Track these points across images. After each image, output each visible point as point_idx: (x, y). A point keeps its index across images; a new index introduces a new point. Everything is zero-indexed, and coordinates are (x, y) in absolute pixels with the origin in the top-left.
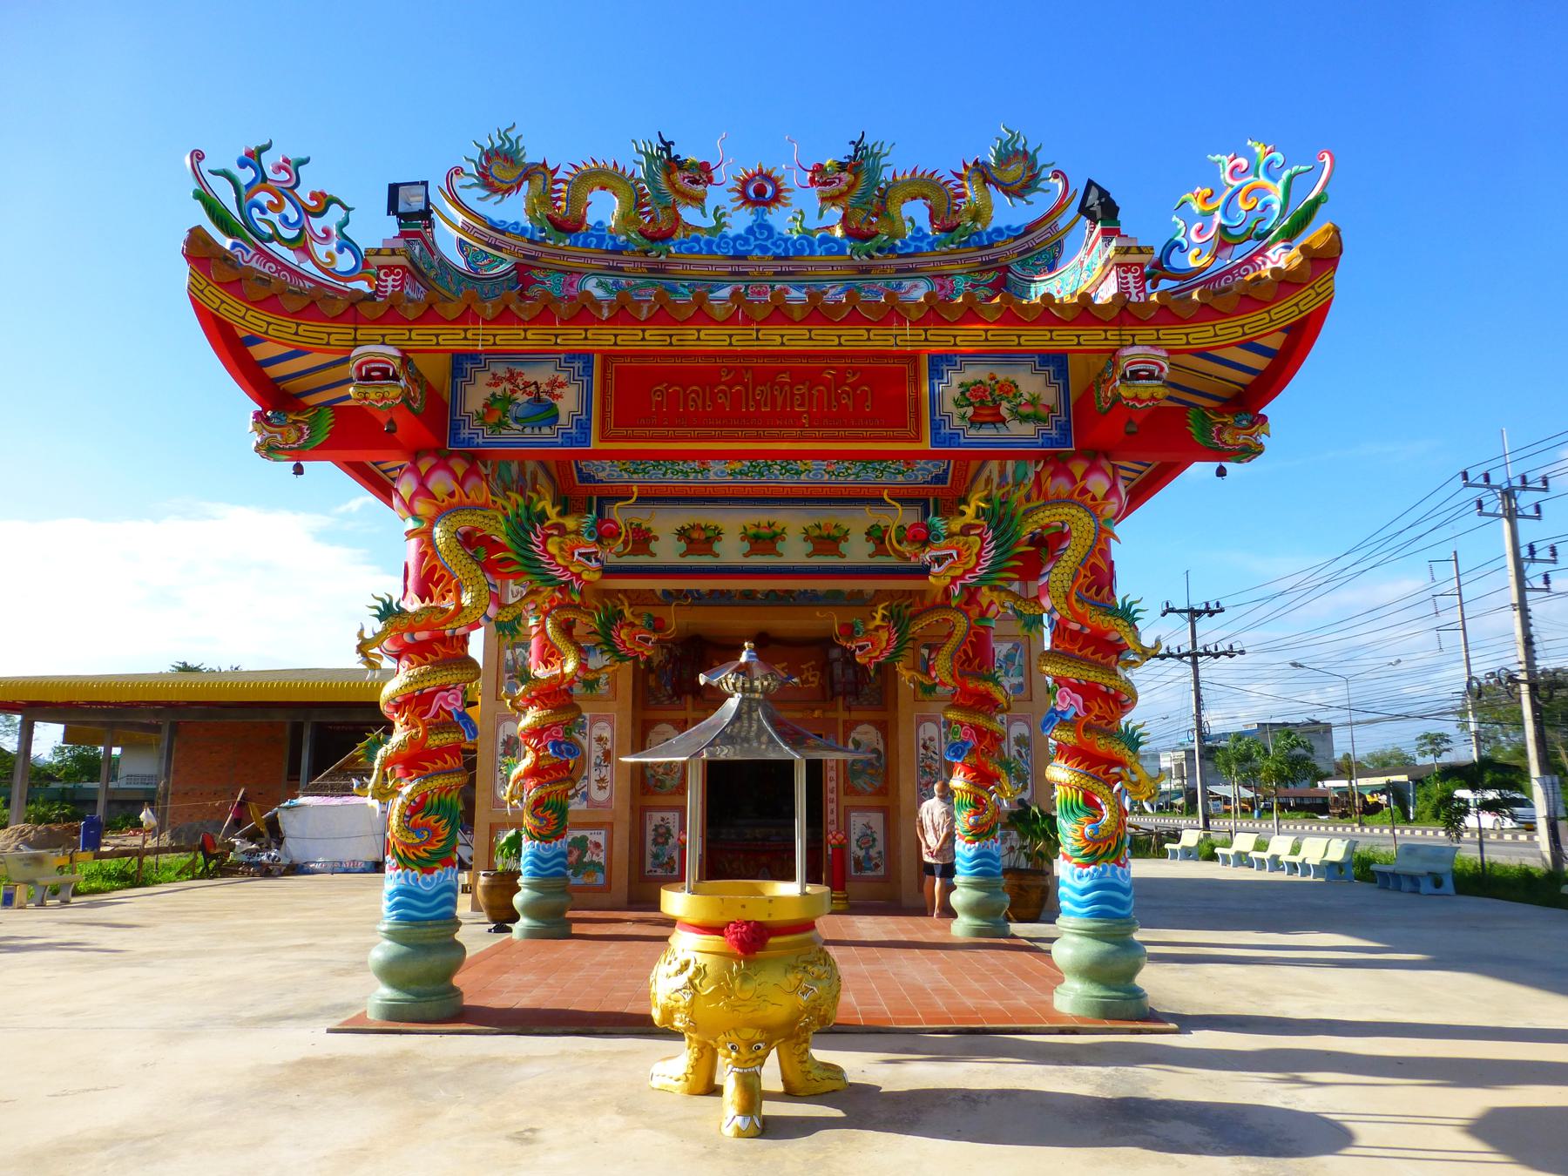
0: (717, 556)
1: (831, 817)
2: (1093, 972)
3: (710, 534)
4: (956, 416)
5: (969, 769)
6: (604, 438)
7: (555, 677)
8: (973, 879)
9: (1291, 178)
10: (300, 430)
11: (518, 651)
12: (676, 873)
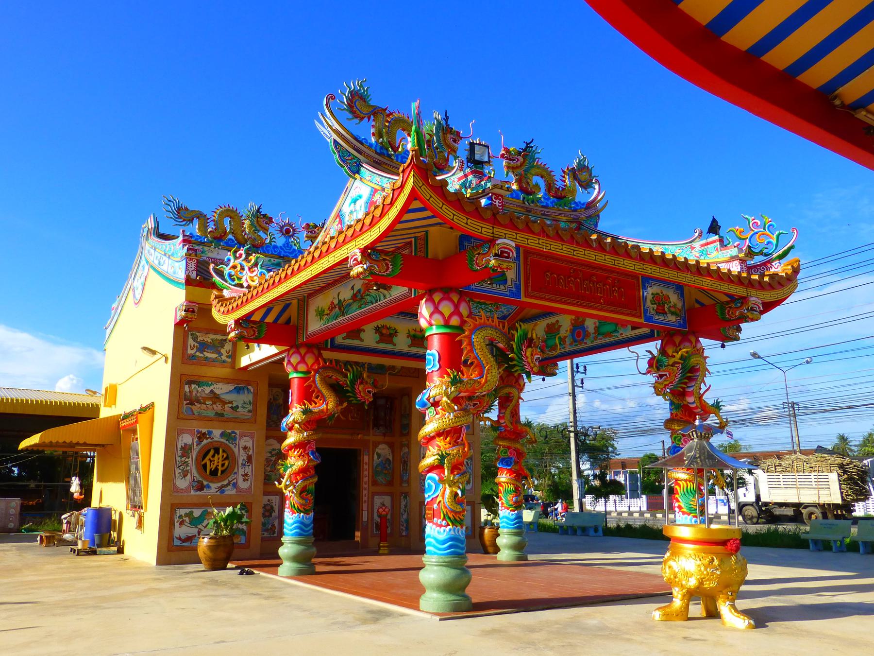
0: (395, 345)
1: (365, 499)
2: (448, 588)
3: (392, 332)
4: (652, 307)
5: (510, 472)
6: (527, 296)
7: (322, 411)
8: (515, 531)
9: (780, 234)
10: (387, 265)
11: (193, 386)
12: (276, 535)
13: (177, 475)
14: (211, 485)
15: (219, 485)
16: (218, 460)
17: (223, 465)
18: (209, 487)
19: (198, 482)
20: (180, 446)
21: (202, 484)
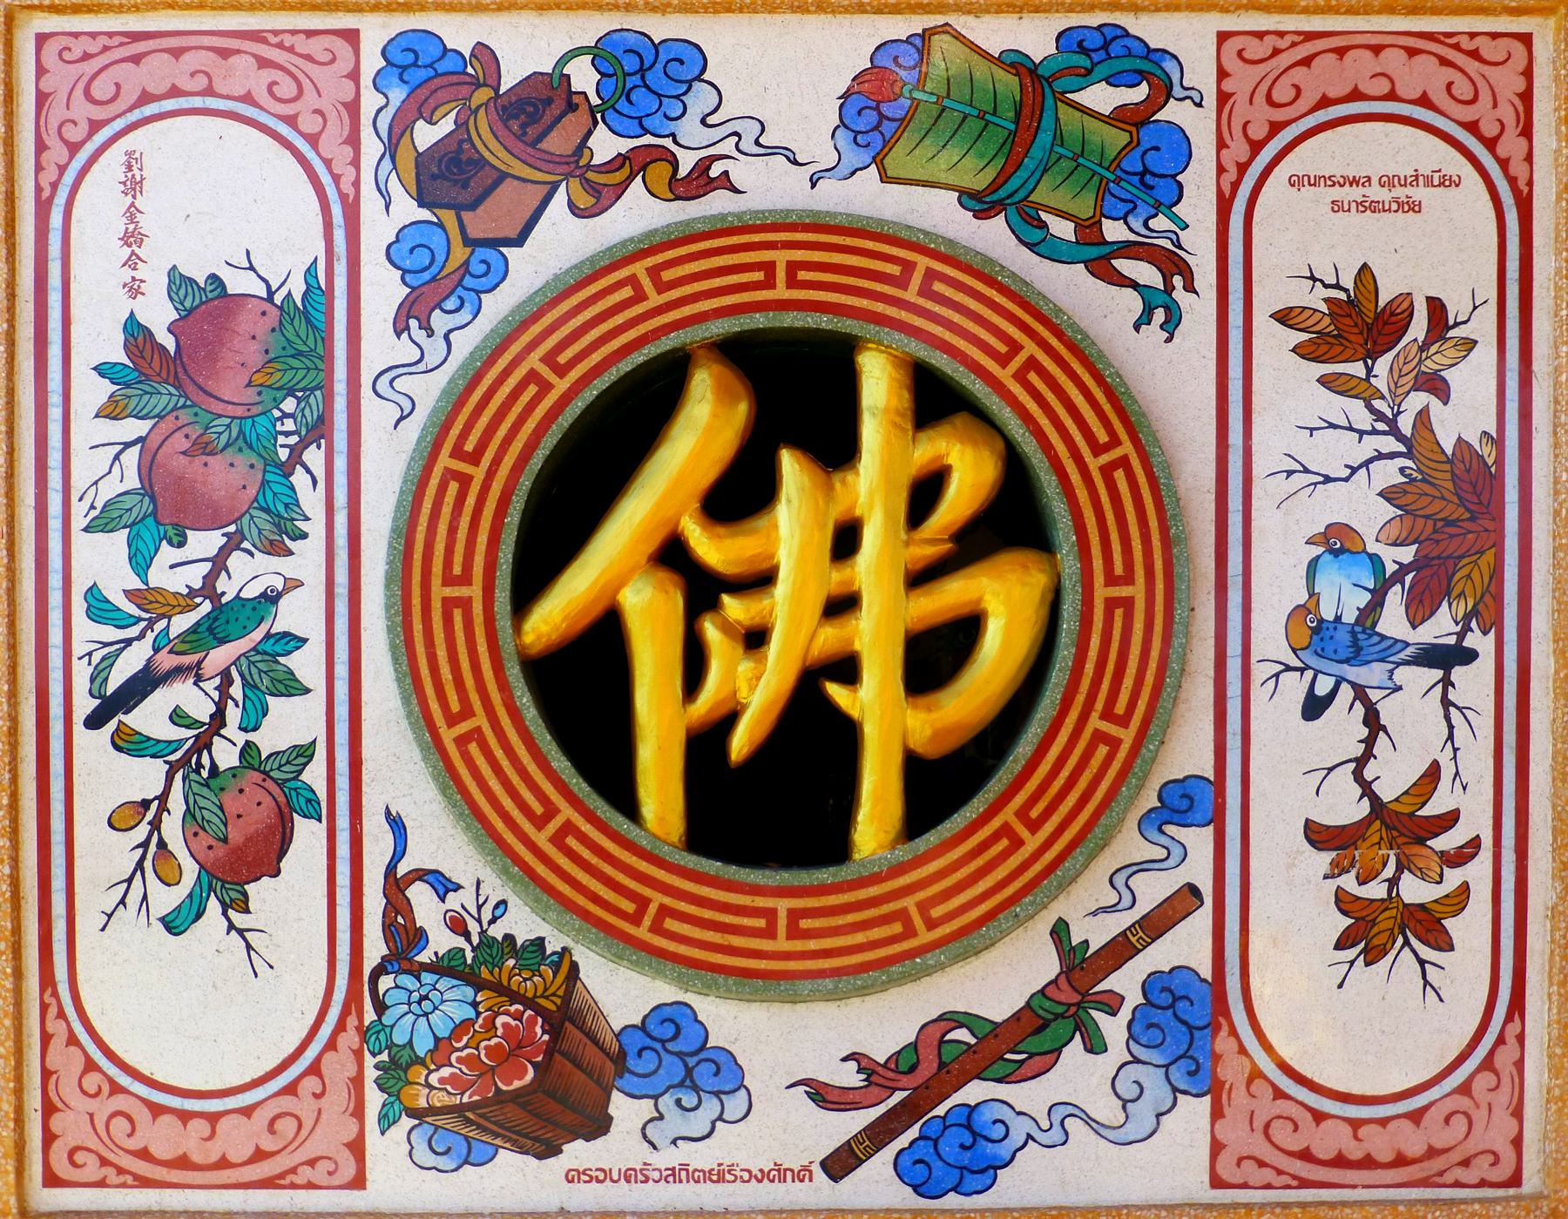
13: (103, 855)
14: (727, 1019)
15: (887, 1022)
16: (832, 574)
17: (935, 656)
18: (689, 1065)
19: (488, 966)
20: (98, 340)
21: (567, 1015)
